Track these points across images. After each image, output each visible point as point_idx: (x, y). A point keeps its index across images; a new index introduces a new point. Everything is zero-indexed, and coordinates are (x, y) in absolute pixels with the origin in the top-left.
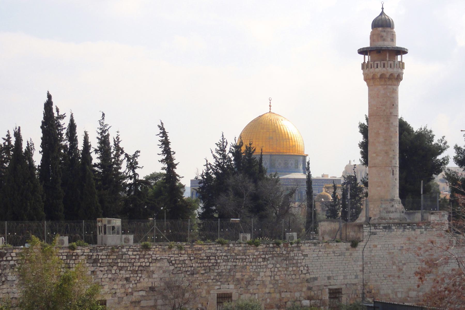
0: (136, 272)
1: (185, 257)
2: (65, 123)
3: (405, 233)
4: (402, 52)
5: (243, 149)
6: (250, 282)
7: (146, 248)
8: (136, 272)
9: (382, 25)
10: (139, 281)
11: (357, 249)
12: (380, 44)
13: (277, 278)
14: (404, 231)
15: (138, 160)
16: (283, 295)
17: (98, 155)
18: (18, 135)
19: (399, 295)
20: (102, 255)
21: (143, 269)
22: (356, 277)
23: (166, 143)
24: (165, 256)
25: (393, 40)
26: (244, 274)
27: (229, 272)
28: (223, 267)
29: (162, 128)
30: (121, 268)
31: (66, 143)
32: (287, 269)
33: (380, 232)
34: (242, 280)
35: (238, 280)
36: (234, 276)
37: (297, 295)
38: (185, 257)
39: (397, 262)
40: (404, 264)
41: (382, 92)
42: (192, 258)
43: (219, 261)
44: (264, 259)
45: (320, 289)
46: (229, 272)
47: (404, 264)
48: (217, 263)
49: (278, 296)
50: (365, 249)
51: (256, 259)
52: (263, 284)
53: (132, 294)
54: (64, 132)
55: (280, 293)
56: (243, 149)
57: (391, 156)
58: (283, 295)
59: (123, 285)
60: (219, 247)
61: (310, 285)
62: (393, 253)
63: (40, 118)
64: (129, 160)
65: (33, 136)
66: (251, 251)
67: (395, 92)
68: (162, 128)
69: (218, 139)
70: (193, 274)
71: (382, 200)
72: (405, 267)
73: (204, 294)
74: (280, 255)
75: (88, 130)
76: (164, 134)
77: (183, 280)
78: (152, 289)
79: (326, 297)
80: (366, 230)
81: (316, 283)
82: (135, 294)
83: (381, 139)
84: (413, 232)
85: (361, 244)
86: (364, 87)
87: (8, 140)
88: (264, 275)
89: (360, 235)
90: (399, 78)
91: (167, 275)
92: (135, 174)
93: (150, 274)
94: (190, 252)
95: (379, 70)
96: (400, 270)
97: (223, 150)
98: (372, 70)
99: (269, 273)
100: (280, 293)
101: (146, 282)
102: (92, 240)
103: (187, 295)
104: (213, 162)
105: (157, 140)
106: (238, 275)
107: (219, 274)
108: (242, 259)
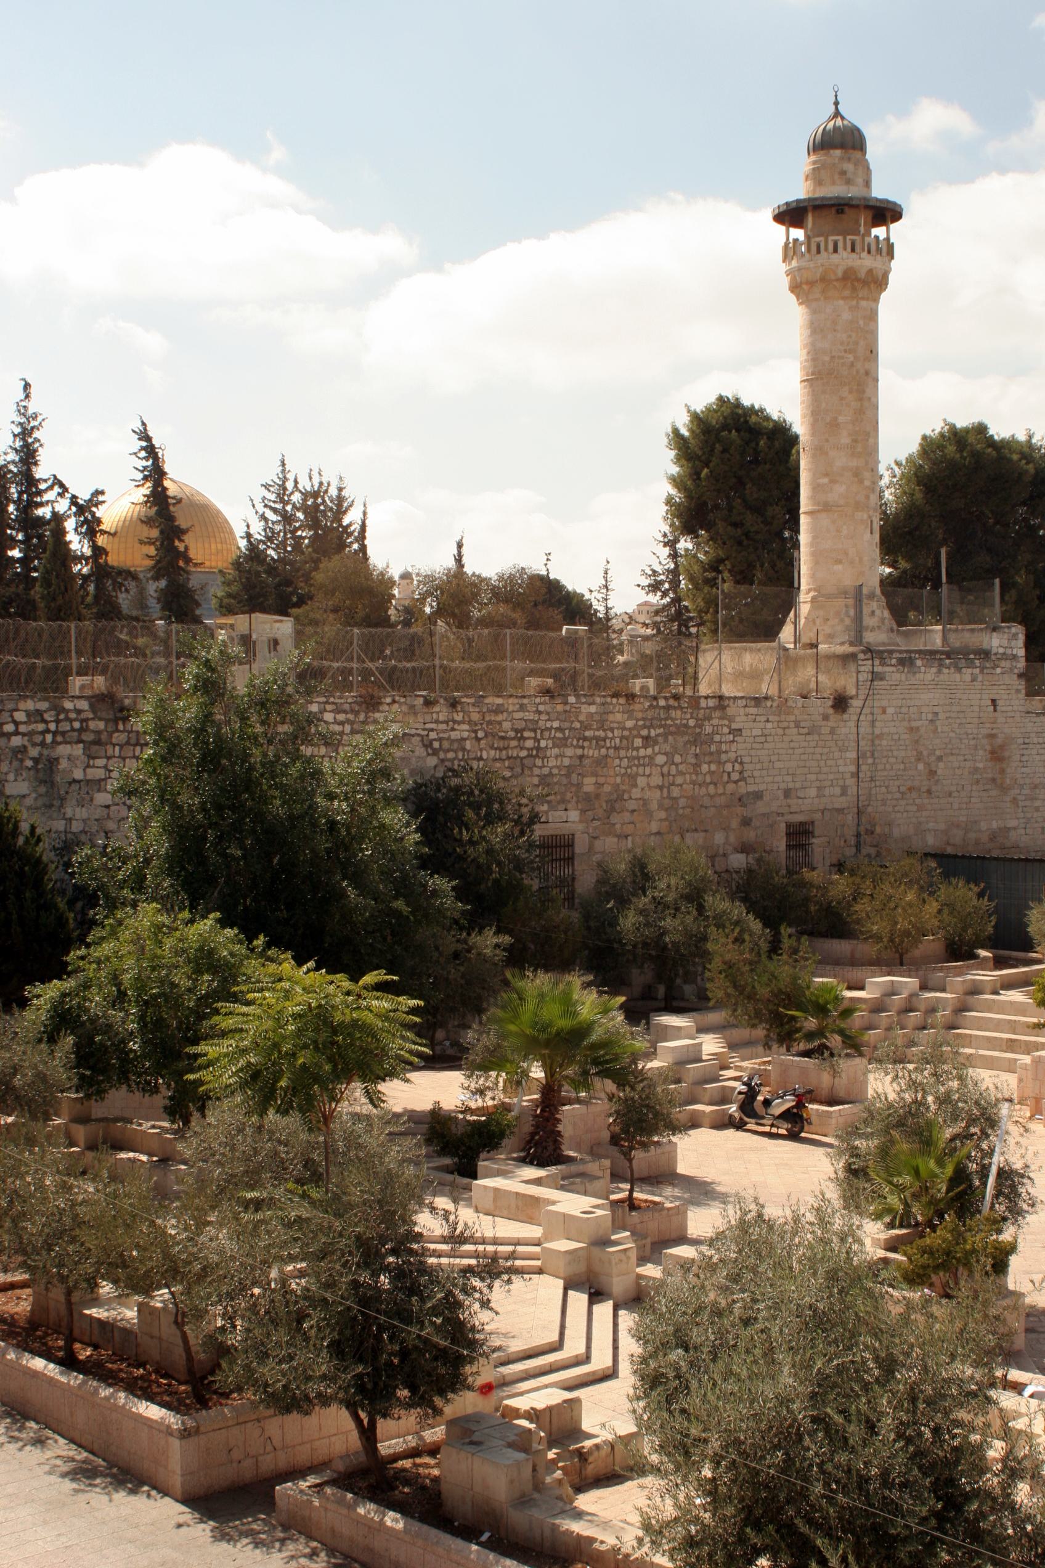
3: (942, 677)
11: (846, 716)
13: (676, 792)
14: (939, 672)
22: (844, 793)
25: (867, 184)
26: (601, 780)
27: (568, 775)
34: (597, 796)
36: (579, 785)
37: (719, 838)
39: (925, 753)
40: (940, 759)
41: (846, 316)
42: (481, 734)
43: (543, 744)
44: (646, 738)
46: (568, 775)
47: (940, 759)
48: (538, 749)
50: (862, 718)
57: (867, 483)
62: (918, 728)
67: (873, 316)
69: (272, 474)
72: (941, 765)
76: (151, 451)
79: (781, 844)
81: (761, 807)
83: (845, 440)
84: (958, 676)
90: (878, 282)
94: (475, 717)
96: (932, 773)
99: (656, 780)
106: (589, 784)
108: (597, 739)
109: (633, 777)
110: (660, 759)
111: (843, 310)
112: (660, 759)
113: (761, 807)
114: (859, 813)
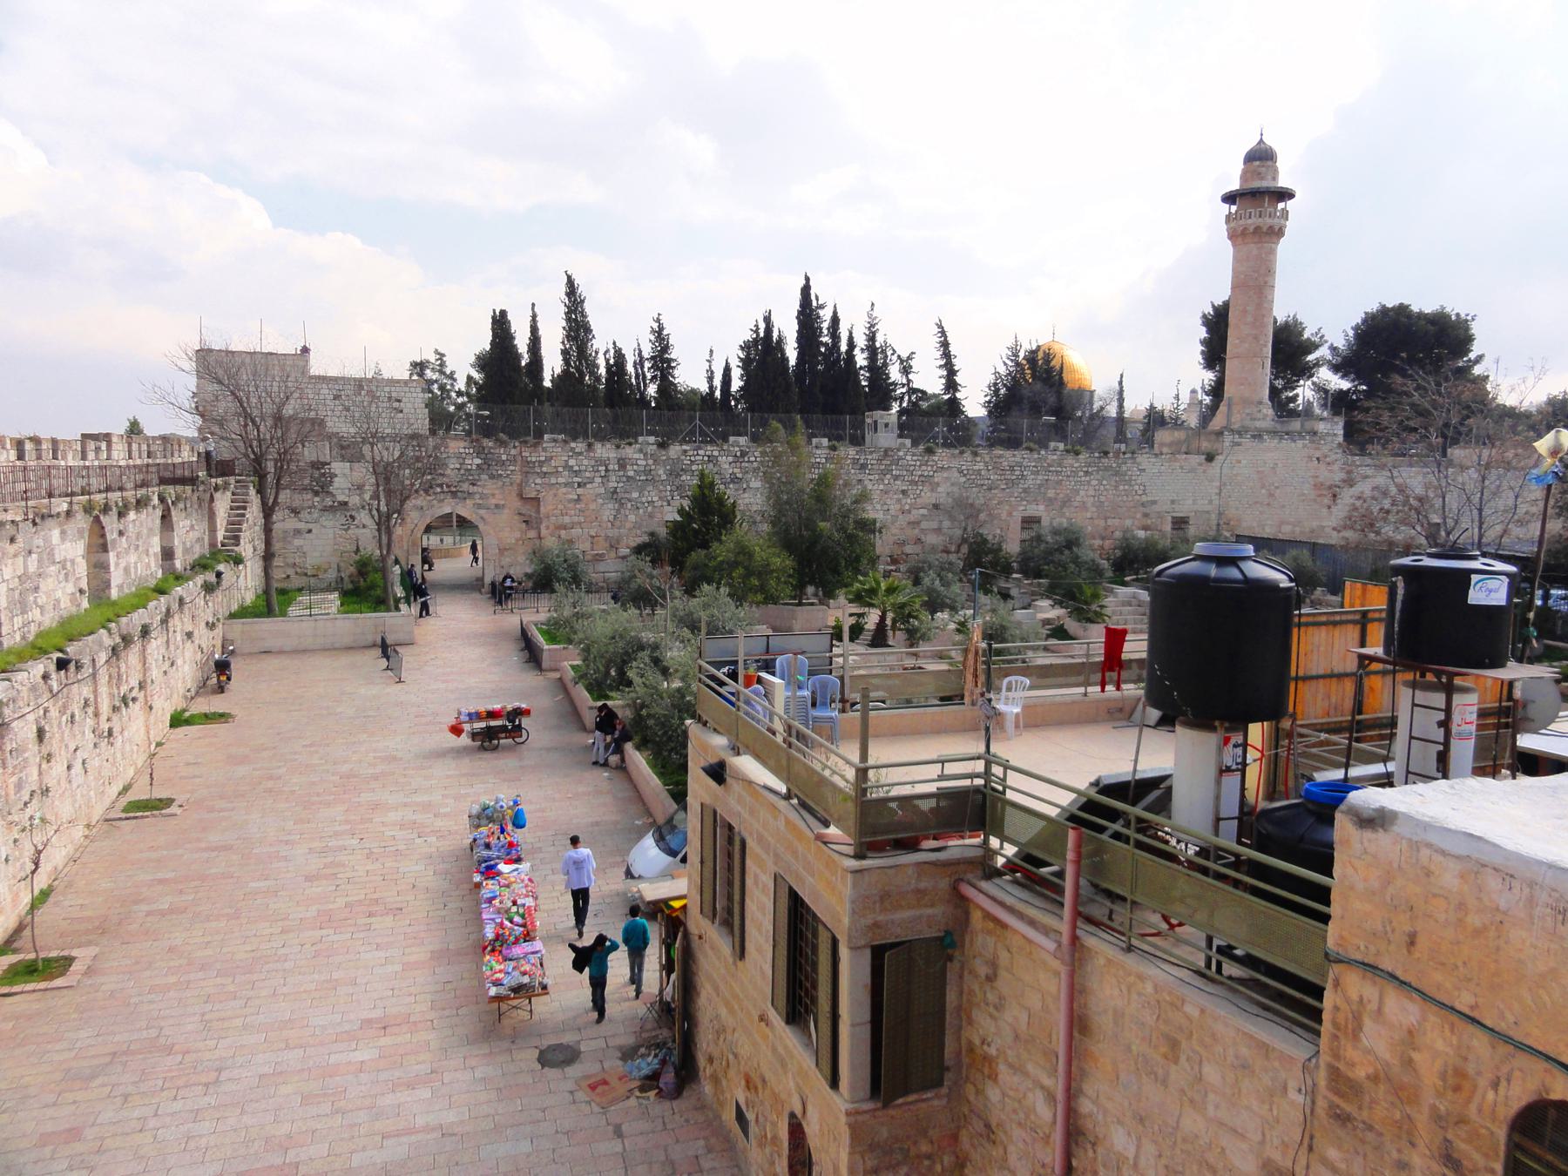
0: (916, 483)
1: (980, 466)
2: (826, 315)
4: (1285, 195)
5: (1040, 355)
6: (1066, 502)
7: (930, 451)
8: (916, 483)
9: (1260, 157)
10: (919, 496)
12: (1257, 184)
13: (1103, 499)
15: (912, 363)
16: (1110, 522)
17: (865, 355)
18: (767, 320)
19: (1268, 530)
20: (872, 459)
21: (926, 480)
22: (1211, 502)
23: (945, 345)
24: (955, 463)
25: (1275, 178)
28: (1031, 481)
29: (940, 326)
30: (896, 478)
31: (825, 339)
32: (1116, 487)
33: (1246, 441)
35: (1050, 500)
37: (1128, 522)
38: (980, 466)
41: (1255, 252)
44: (1087, 473)
45: (1160, 516)
49: (1102, 523)
51: (1075, 473)
52: (1084, 506)
53: (909, 512)
54: (825, 325)
55: (1106, 519)
56: (1040, 355)
58: (1110, 522)
59: (899, 501)
60: (1026, 454)
61: (1147, 510)
63: (797, 306)
64: (902, 362)
65: (788, 329)
66: (1070, 460)
67: (1273, 252)
68: (940, 326)
69: (1011, 343)
70: (990, 489)
71: (1246, 402)
73: (1004, 516)
74: (1106, 469)
75: (853, 325)
76: (943, 333)
77: (977, 497)
78: (936, 506)
79: (1168, 527)
80: (1228, 438)
81: (1156, 508)
82: (914, 512)
83: (1250, 319)
85: (1219, 458)
86: (1227, 250)
87: (756, 331)
88: (1085, 495)
89: (1217, 446)
90: (1279, 233)
91: (955, 489)
92: (909, 381)
93: (934, 487)
95: (1253, 222)
97: (1016, 355)
98: (1242, 222)
99: (1091, 492)
100: (1106, 519)
101: (928, 497)
102: (858, 441)
103: (982, 516)
104: (1002, 370)
105: (935, 341)
106: (1051, 493)
107: (1025, 491)
109: (1077, 492)
110: (1094, 482)
111: (1253, 248)
112: (1094, 482)
113: (1156, 508)
114: (1220, 514)
